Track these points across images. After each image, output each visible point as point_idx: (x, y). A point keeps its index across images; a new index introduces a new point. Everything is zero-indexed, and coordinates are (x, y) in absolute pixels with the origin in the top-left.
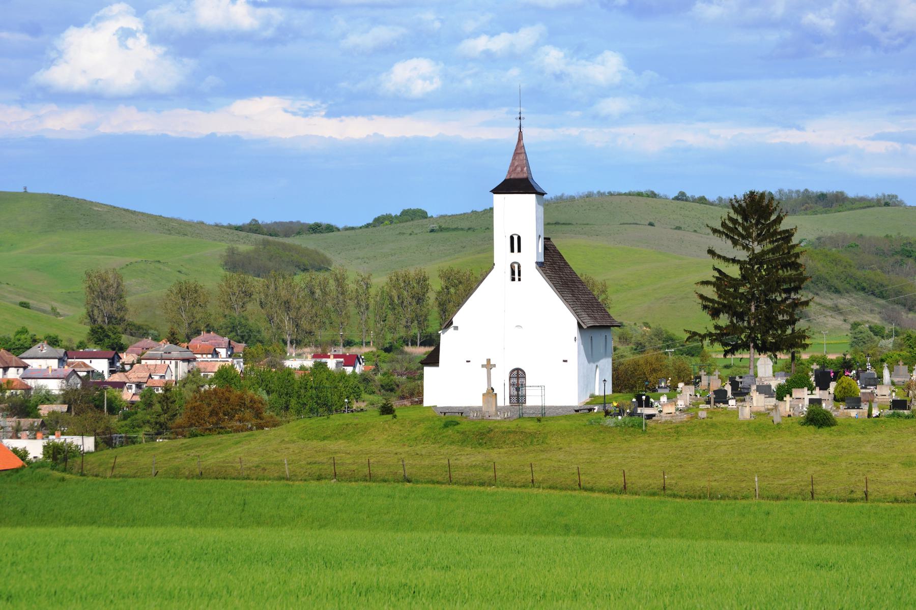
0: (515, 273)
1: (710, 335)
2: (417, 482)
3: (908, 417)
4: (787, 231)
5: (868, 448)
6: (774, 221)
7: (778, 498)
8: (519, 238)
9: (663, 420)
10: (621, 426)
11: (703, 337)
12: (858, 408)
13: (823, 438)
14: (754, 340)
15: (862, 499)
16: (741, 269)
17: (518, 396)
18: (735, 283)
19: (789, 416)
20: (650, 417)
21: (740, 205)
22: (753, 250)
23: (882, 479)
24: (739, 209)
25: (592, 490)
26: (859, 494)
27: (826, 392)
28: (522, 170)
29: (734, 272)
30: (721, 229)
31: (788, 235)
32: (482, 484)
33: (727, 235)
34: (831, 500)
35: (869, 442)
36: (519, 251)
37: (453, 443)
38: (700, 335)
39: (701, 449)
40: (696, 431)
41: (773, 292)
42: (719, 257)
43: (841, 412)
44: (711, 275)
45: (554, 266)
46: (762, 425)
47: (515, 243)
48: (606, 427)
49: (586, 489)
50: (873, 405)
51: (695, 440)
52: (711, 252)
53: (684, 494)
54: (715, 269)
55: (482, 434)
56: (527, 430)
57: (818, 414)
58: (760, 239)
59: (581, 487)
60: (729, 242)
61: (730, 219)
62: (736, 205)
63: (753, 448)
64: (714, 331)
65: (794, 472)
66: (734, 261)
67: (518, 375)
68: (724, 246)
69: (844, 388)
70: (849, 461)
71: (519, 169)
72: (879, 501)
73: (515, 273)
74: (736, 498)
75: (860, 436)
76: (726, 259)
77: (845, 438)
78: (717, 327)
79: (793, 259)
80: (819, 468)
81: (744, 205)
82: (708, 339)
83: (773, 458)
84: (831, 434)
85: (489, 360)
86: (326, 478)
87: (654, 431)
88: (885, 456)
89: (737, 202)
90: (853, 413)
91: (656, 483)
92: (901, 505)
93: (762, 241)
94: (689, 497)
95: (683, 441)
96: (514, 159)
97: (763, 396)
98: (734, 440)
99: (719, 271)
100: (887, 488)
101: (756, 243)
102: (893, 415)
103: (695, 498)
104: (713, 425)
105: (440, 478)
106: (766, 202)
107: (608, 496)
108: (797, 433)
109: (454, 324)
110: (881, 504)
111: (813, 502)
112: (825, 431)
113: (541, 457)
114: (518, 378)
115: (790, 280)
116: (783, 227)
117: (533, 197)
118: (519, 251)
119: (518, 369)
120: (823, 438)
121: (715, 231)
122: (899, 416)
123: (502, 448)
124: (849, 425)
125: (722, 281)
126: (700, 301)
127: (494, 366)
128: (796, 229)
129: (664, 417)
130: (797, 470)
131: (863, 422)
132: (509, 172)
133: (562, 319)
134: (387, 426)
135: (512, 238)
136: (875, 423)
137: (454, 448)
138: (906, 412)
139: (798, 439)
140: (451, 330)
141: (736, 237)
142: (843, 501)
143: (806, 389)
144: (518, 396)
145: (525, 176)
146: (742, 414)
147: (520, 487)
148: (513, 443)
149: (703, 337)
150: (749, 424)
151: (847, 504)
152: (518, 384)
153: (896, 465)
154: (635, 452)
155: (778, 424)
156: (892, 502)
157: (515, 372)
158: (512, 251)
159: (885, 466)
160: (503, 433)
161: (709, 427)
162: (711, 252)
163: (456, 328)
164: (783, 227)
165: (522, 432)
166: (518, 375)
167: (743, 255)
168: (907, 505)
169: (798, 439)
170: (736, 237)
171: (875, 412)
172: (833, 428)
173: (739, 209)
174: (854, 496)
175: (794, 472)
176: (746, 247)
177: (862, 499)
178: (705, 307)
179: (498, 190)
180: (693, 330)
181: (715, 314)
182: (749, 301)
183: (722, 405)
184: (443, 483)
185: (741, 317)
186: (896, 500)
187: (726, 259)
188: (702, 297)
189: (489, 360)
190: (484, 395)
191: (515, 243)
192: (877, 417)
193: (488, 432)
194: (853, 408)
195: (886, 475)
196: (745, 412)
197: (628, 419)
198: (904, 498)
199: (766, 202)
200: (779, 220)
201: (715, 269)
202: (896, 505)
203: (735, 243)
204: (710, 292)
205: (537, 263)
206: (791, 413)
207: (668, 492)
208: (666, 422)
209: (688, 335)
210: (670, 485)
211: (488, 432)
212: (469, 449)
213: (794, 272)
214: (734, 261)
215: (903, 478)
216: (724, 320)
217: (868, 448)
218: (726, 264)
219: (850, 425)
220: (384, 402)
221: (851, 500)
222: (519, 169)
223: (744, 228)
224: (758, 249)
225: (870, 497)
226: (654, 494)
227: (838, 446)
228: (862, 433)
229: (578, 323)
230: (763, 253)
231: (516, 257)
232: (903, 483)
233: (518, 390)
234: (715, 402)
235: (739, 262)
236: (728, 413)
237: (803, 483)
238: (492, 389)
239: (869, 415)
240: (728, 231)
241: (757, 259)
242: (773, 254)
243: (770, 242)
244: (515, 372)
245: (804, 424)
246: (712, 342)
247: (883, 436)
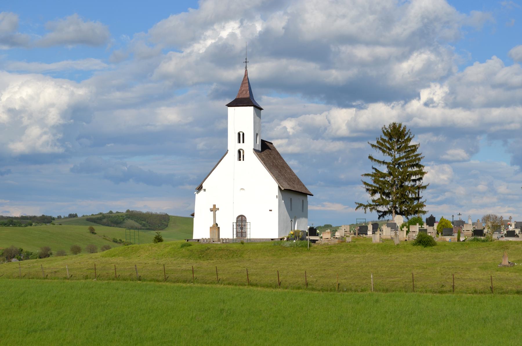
0: (240, 155)
1: (370, 205)
2: (145, 280)
3: (483, 241)
4: (413, 146)
5: (457, 259)
6: (407, 139)
7: (387, 291)
8: (243, 134)
9: (323, 243)
10: (294, 247)
11: (366, 207)
12: (451, 235)
13: (426, 253)
14: (395, 208)
15: (450, 291)
16: (388, 167)
17: (242, 232)
18: (384, 176)
19: (406, 240)
20: (314, 241)
21: (387, 131)
22: (395, 157)
23: (466, 277)
24: (386, 133)
25: (256, 285)
26: (448, 287)
27: (432, 228)
28: (246, 93)
29: (384, 169)
30: (377, 145)
31: (414, 148)
32: (185, 282)
33: (380, 148)
34: (426, 292)
35: (457, 255)
36: (243, 142)
37: (183, 257)
38: (364, 206)
39: (342, 260)
40: (343, 249)
41: (406, 181)
42: (375, 160)
43: (439, 239)
44: (372, 171)
45: (265, 149)
46: (387, 246)
47: (241, 137)
48: (284, 247)
49: (252, 285)
50: (461, 235)
51: (341, 255)
52: (370, 157)
53: (320, 288)
54: (373, 168)
55: (202, 251)
56: (231, 249)
57: (425, 238)
58: (399, 150)
59: (251, 284)
60: (381, 152)
61: (382, 139)
62: (385, 131)
63: (378, 259)
64: (372, 203)
65: (403, 273)
66: (384, 163)
67: (241, 221)
68: (378, 155)
69: (443, 226)
70: (442, 266)
71: (244, 92)
72: (462, 292)
73: (240, 155)
74: (356, 291)
75: (451, 252)
76: (379, 162)
77: (441, 253)
78: (373, 201)
79: (417, 162)
80: (421, 271)
81: (389, 131)
82: (368, 208)
83: (390, 265)
84: (432, 251)
85: (215, 206)
86: (90, 278)
87: (315, 249)
88: (468, 263)
89: (386, 129)
90: (448, 238)
91: (301, 280)
92: (480, 295)
93: (400, 151)
94: (323, 290)
95: (333, 255)
96: (242, 86)
97: (389, 229)
98: (367, 254)
99: (376, 169)
100: (469, 283)
101: (396, 152)
102: (474, 240)
103: (327, 291)
104: (355, 246)
105: (160, 278)
106: (402, 129)
107: (268, 290)
108: (410, 251)
109: (204, 188)
110: (464, 295)
111: (413, 293)
112: (428, 249)
113: (235, 265)
114: (242, 221)
115: (415, 173)
116: (411, 143)
117: (252, 108)
118: (243, 142)
119: (242, 216)
120: (426, 253)
121: (373, 146)
122: (478, 240)
123: (213, 260)
124: (445, 245)
125: (377, 174)
126: (364, 186)
127: (218, 209)
128: (419, 145)
129: (323, 241)
130: (404, 272)
131: (455, 243)
132: (239, 95)
133: (268, 186)
134: (150, 248)
135: (239, 134)
136: (462, 244)
137: (183, 260)
138: (482, 238)
139: (409, 254)
140: (202, 192)
141: (385, 149)
142: (436, 293)
143: (418, 224)
144: (242, 232)
145: (248, 96)
146: (374, 239)
147: (209, 284)
148: (221, 257)
149: (366, 207)
150: (378, 245)
151: (438, 295)
152: (242, 225)
153: (476, 269)
154: (297, 262)
155: (398, 245)
156: (473, 293)
157: (240, 218)
158: (239, 142)
159: (468, 270)
160: (216, 250)
161: (352, 247)
162: (370, 157)
163: (205, 190)
164: (411, 143)
165: (227, 250)
166: (241, 221)
167: (389, 159)
168: (483, 295)
169: (409, 254)
170: (385, 149)
171: (462, 239)
172: (433, 247)
173: (386, 133)
174: (444, 289)
175: (403, 273)
176: (390, 155)
177: (450, 291)
178: (368, 190)
179: (230, 105)
180: (360, 203)
181: (374, 192)
182: (392, 186)
183: (364, 236)
184: (161, 281)
185: (388, 195)
186: (476, 292)
187: (379, 162)
188: (365, 183)
189: (215, 206)
190: (211, 228)
191: (241, 137)
192: (464, 241)
193: (206, 250)
194: (449, 235)
195: (469, 275)
196: (376, 238)
197: (299, 242)
198: (482, 291)
199: (402, 129)
200: (409, 139)
201: (373, 168)
202: (475, 295)
203: (384, 152)
204: (370, 180)
205: (254, 150)
206: (407, 239)
207: (310, 287)
208: (324, 244)
209: (358, 205)
210: (312, 282)
211: (206, 250)
212: (192, 261)
213: (417, 169)
214: (384, 163)
215: (481, 277)
216: (377, 196)
217: (457, 259)
218: (379, 164)
219: (445, 245)
220: (157, 235)
221: (441, 292)
222: (244, 92)
223: (390, 144)
224: (397, 156)
225: (456, 290)
226: (299, 288)
227: (436, 258)
228: (453, 250)
229: (279, 187)
230: (400, 158)
231: (241, 146)
232: (480, 280)
233: (242, 228)
234: (359, 234)
235: (386, 163)
236: (366, 239)
237: (407, 280)
238: (217, 224)
239: (459, 240)
240: (381, 146)
241: (396, 162)
242: (406, 159)
243: (405, 152)
244: (240, 218)
245: (414, 245)
246: (371, 209)
247: (467, 252)
